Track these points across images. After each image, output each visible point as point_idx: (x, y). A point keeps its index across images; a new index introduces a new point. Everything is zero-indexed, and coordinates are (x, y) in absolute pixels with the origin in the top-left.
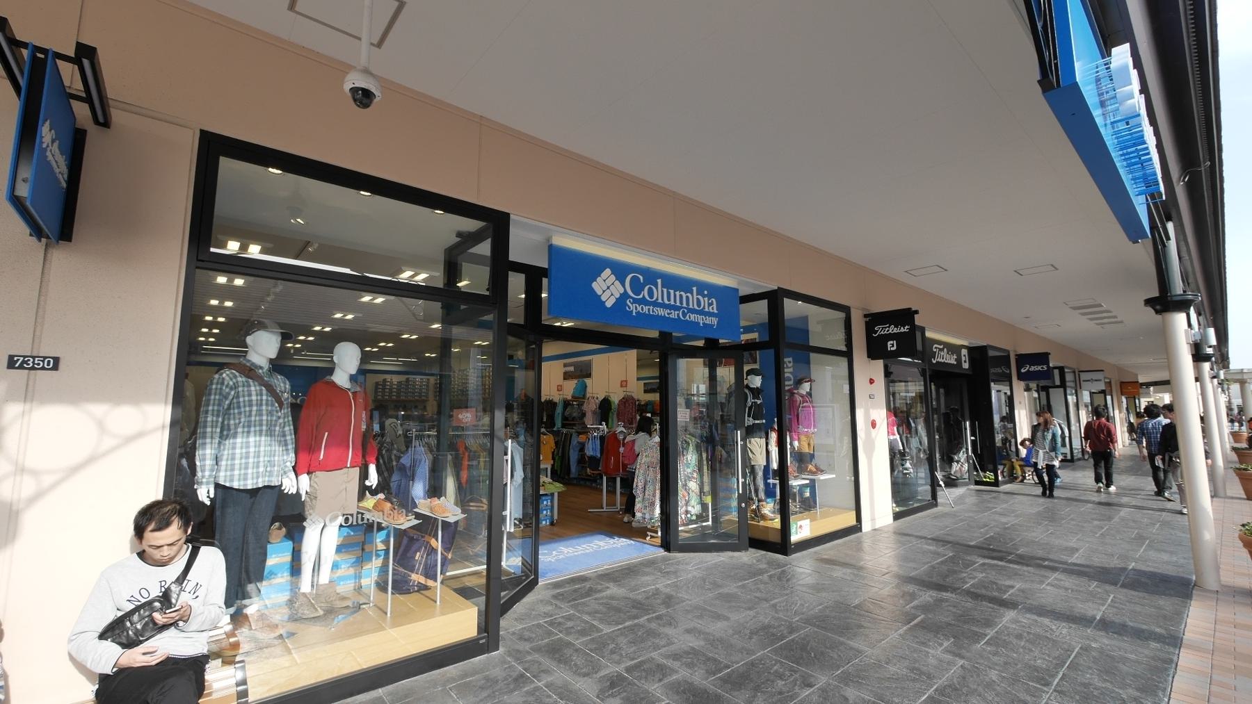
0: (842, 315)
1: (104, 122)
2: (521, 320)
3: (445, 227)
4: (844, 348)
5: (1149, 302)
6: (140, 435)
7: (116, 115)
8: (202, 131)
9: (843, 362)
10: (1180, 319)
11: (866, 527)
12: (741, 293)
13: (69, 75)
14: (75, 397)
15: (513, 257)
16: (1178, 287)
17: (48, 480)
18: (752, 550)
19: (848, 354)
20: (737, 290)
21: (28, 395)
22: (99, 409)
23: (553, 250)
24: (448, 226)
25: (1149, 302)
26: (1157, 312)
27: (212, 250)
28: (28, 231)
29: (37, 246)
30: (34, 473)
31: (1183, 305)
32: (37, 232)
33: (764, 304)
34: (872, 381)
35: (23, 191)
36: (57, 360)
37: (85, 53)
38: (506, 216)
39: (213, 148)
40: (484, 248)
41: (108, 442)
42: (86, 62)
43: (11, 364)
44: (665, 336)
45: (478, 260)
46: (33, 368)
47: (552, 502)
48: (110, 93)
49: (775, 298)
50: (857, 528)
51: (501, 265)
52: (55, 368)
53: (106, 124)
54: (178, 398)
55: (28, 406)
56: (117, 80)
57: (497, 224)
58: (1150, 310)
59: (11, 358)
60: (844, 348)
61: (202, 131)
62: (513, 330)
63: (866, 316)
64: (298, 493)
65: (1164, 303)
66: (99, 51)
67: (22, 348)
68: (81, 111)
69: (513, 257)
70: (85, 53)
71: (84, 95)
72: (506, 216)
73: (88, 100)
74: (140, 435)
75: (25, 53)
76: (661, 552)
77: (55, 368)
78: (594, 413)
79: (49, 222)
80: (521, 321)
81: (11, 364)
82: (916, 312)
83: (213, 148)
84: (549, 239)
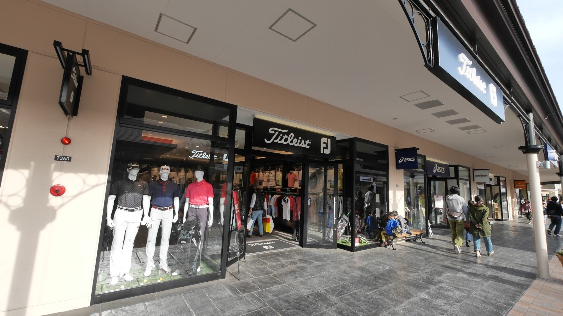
1: (89, 73)
2: (243, 147)
5: (520, 148)
6: (97, 185)
7: (94, 71)
8: (123, 76)
10: (534, 157)
13: (79, 59)
15: (238, 121)
16: (534, 142)
18: (338, 249)
21: (61, 170)
22: (84, 175)
23: (256, 120)
26: (524, 153)
28: (63, 112)
31: (535, 150)
32: (66, 113)
34: (57, 191)
35: (64, 100)
36: (70, 158)
37: (85, 53)
38: (237, 106)
39: (127, 82)
41: (86, 188)
42: (86, 56)
43: (56, 159)
46: (63, 160)
47: (472, 281)
48: (92, 63)
51: (233, 126)
52: (70, 160)
53: (90, 74)
55: (60, 173)
56: (94, 59)
57: (232, 109)
59: (56, 156)
61: (123, 76)
63: (395, 150)
65: (528, 149)
66: (90, 52)
68: (82, 70)
69: (238, 121)
70: (85, 53)
71: (83, 64)
73: (85, 66)
74: (97, 185)
75: (66, 53)
76: (300, 247)
77: (70, 160)
78: (511, 180)
81: (56, 159)
82: (418, 149)
84: (254, 115)
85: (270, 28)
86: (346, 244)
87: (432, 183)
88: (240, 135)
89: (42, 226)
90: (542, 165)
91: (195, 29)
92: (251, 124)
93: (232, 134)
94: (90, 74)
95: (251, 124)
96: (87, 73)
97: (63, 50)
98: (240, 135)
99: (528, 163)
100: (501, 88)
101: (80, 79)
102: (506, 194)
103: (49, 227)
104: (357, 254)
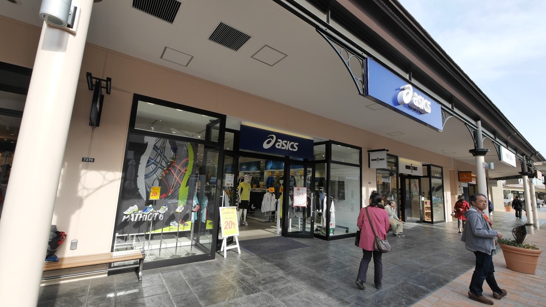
0: (359, 151)
1: (108, 92)
3: (206, 119)
4: (359, 164)
5: (471, 151)
7: (112, 91)
9: (357, 170)
10: (482, 159)
11: (447, 221)
12: (314, 142)
13: (104, 83)
14: (98, 169)
15: (228, 126)
17: (91, 191)
18: (315, 238)
19: (360, 166)
20: (313, 141)
21: (87, 168)
22: (104, 172)
23: (242, 127)
24: (206, 119)
25: (471, 151)
26: (474, 155)
27: (240, 150)
29: (90, 128)
30: (87, 189)
31: (483, 153)
33: (325, 145)
36: (94, 159)
37: (109, 80)
40: (218, 125)
41: (106, 182)
43: (83, 160)
44: (287, 157)
45: (216, 128)
49: (328, 144)
50: (444, 221)
51: (223, 129)
53: (109, 94)
54: (125, 170)
56: (113, 83)
57: (222, 118)
58: (471, 155)
60: (359, 164)
62: (228, 153)
64: (143, 297)
65: (477, 152)
67: (86, 156)
69: (228, 126)
70: (109, 80)
72: (225, 116)
77: (93, 161)
79: (94, 121)
80: (232, 150)
81: (83, 160)
83: (137, 98)
85: (252, 57)
86: (321, 234)
87: (407, 181)
88: (229, 136)
89: (72, 212)
90: (488, 166)
91: (193, 57)
92: (239, 129)
93: (222, 136)
94: (109, 94)
95: (239, 129)
96: (107, 93)
97: (92, 78)
98: (229, 136)
99: (476, 161)
100: (450, 98)
101: (102, 97)
102: (441, 188)
103: (77, 212)
104: (332, 242)
